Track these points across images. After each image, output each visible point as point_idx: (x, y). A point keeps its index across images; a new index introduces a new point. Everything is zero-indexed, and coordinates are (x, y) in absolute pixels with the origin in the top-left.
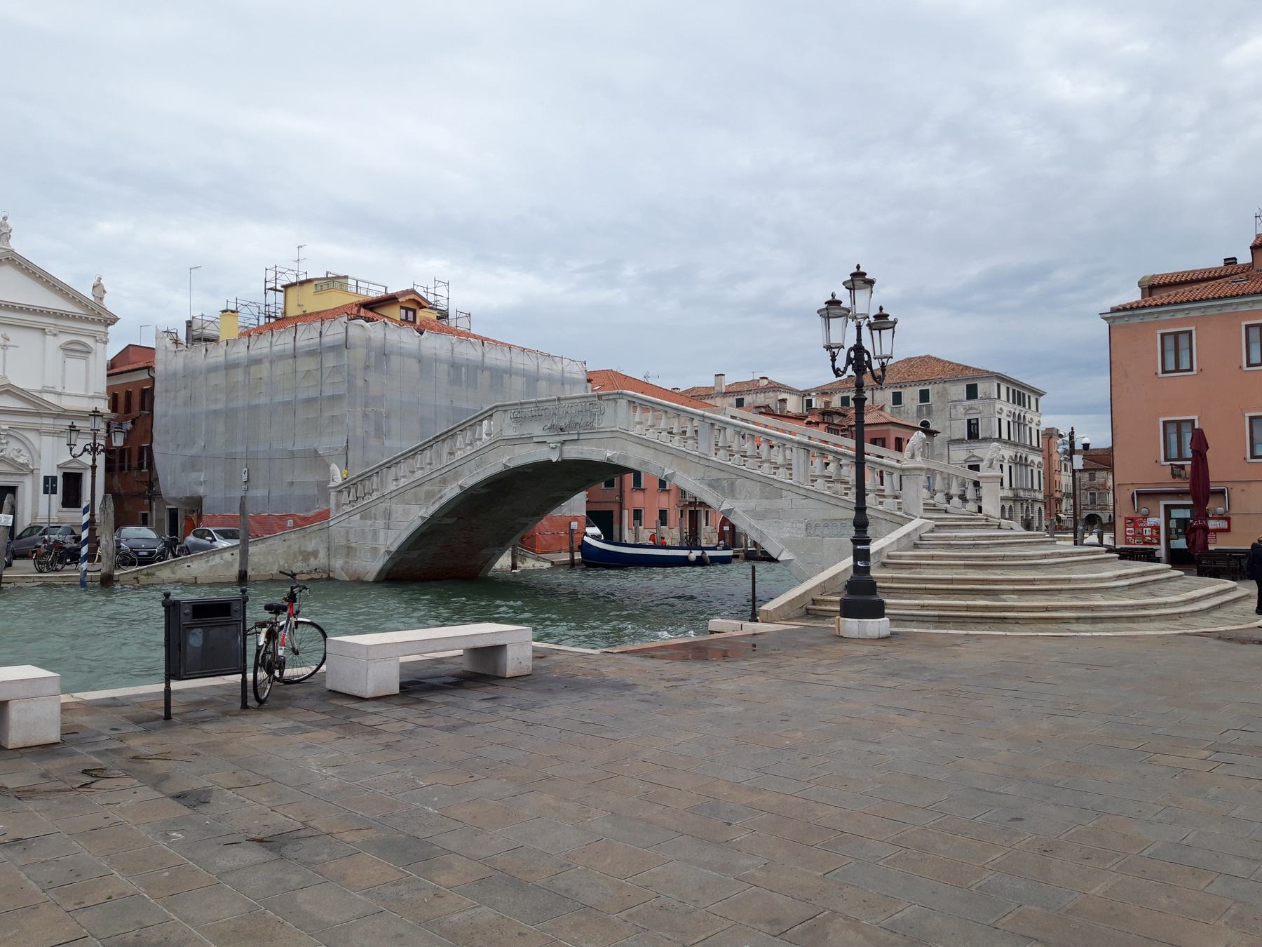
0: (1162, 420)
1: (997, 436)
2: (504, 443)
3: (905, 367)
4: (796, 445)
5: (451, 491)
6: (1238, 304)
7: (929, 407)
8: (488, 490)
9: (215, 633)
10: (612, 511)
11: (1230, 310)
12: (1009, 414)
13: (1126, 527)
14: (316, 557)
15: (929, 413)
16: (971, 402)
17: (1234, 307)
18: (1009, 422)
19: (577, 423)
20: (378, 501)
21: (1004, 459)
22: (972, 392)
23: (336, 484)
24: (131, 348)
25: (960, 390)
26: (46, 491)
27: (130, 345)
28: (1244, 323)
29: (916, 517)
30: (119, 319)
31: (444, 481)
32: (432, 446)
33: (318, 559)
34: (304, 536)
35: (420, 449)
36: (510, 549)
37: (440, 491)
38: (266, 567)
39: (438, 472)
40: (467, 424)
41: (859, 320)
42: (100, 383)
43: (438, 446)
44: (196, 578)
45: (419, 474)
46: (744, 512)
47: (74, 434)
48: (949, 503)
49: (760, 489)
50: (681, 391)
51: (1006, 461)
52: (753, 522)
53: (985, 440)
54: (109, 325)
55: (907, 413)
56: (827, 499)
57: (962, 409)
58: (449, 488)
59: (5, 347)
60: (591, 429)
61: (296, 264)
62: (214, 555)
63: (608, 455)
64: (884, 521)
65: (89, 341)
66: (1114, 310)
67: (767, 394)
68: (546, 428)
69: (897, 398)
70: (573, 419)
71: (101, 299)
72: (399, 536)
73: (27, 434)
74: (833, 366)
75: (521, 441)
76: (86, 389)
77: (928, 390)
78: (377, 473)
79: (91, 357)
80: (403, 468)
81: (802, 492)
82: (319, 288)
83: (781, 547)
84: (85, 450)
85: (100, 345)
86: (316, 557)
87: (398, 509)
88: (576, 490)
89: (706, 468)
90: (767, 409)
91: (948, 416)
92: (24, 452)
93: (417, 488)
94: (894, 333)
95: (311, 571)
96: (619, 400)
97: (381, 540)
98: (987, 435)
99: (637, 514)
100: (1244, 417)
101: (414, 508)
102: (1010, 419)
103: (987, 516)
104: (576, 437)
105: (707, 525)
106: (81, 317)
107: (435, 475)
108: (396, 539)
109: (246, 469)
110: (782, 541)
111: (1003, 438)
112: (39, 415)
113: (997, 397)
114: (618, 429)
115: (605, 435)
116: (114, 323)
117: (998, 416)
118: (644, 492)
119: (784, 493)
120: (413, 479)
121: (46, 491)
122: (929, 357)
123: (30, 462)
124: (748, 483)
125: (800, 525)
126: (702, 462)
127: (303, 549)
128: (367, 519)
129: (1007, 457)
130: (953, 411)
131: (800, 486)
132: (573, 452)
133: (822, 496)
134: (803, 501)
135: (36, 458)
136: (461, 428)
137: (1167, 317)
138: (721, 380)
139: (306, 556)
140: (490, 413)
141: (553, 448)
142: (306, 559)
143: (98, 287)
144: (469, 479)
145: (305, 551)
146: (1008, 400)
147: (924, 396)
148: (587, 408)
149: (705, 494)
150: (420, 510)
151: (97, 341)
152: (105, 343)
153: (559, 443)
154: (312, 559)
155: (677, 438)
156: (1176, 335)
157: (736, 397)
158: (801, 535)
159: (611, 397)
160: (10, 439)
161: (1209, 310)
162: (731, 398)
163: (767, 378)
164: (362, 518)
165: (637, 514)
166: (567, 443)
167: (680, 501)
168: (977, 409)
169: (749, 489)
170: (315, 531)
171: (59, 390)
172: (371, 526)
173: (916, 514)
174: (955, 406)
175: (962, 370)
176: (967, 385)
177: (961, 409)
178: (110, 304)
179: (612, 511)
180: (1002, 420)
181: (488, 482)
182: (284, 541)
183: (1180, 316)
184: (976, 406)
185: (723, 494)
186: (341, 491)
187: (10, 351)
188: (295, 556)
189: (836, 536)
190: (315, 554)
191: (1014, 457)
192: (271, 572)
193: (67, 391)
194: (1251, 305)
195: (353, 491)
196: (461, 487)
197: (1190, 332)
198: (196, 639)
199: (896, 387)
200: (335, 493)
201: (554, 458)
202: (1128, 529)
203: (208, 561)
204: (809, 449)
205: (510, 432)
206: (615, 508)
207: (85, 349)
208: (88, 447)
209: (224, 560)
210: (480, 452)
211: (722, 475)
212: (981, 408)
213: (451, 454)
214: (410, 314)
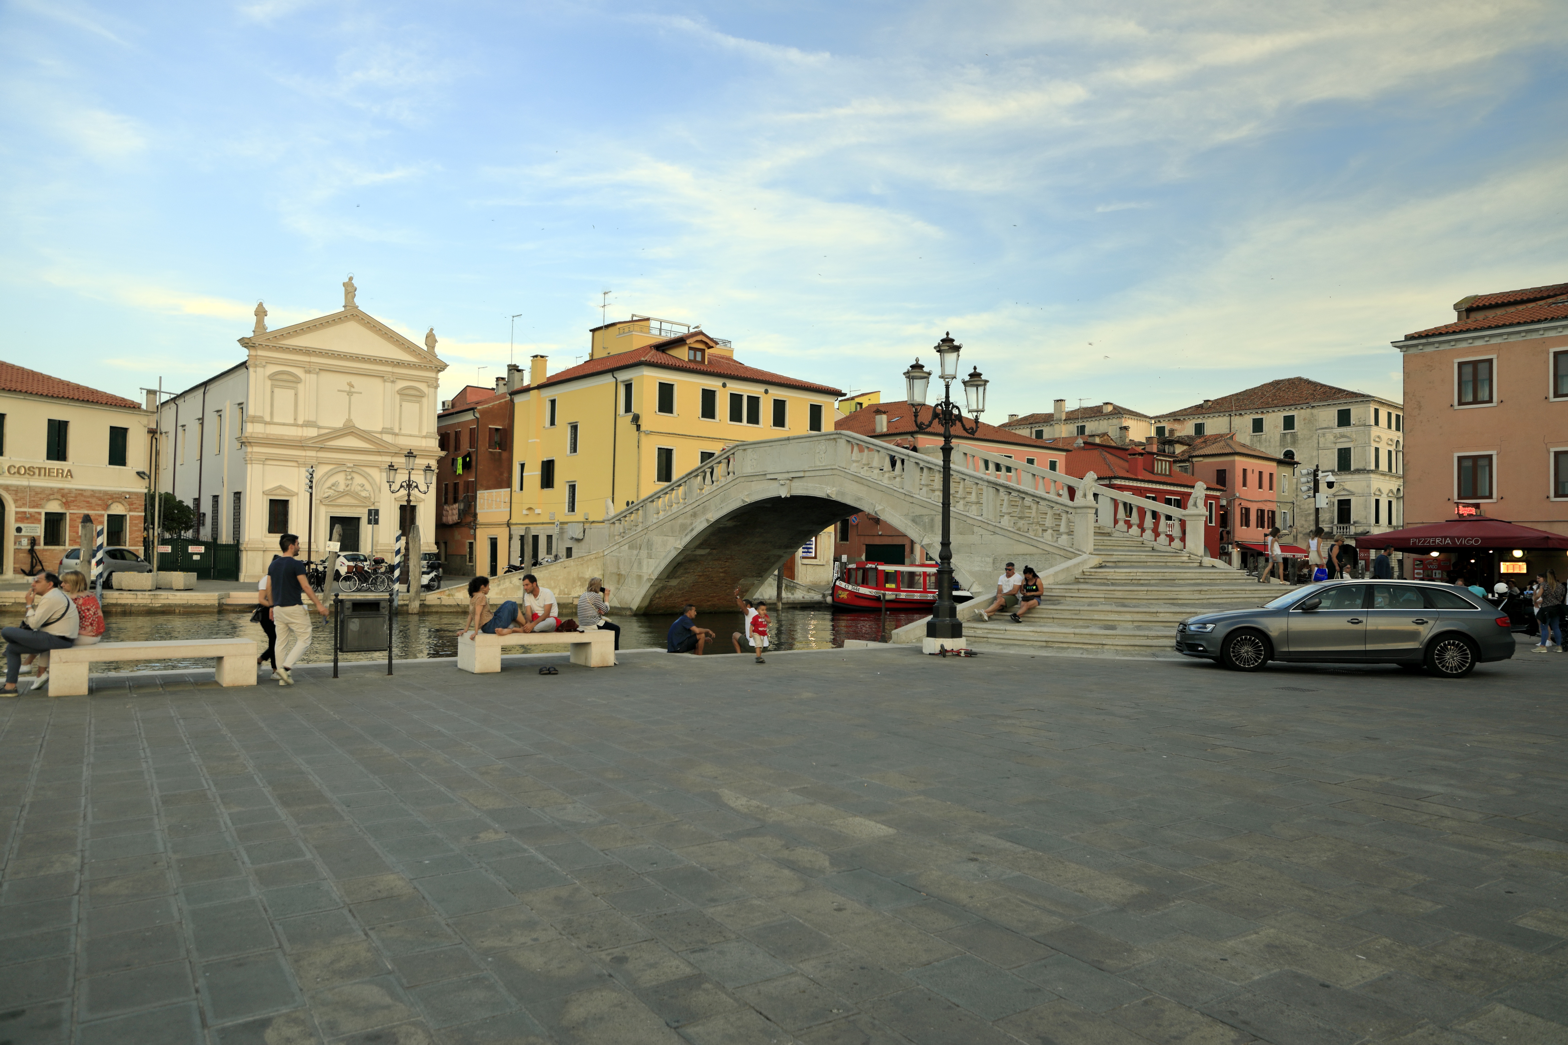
0: (1456, 455)
1: (1373, 467)
3: (1271, 391)
4: (986, 484)
5: (700, 525)
6: (1545, 329)
7: (1294, 436)
9: (368, 621)
10: (904, 545)
11: (1535, 336)
12: (1390, 443)
13: (1414, 569)
15: (1294, 441)
16: (1343, 430)
17: (1541, 332)
18: (1390, 452)
21: (1382, 493)
22: (1344, 419)
24: (468, 388)
25: (1328, 415)
26: (369, 522)
27: (467, 386)
28: (1457, 361)
29: (1085, 553)
31: (695, 515)
32: (685, 482)
34: (582, 564)
37: (692, 524)
41: (947, 380)
42: (431, 426)
47: (392, 472)
48: (1156, 540)
50: (1019, 417)
51: (1384, 495)
53: (1358, 471)
54: (439, 371)
55: (1269, 442)
56: (1011, 535)
57: (1332, 437)
58: (699, 521)
59: (350, 394)
61: (603, 309)
64: (1058, 556)
66: (1409, 338)
67: (1110, 421)
69: (1258, 426)
71: (433, 347)
73: (368, 470)
74: (916, 421)
75: (757, 478)
76: (420, 430)
77: (1293, 416)
79: (425, 400)
81: (990, 528)
82: (621, 331)
83: (972, 579)
84: (402, 486)
87: (657, 540)
89: (911, 505)
90: (1106, 437)
91: (1316, 445)
92: (368, 486)
94: (984, 390)
97: (645, 569)
98: (1360, 466)
100: (1549, 452)
101: (671, 540)
102: (1393, 448)
103: (1190, 553)
107: (687, 509)
108: (656, 568)
112: (379, 453)
113: (1372, 422)
115: (826, 473)
117: (1375, 445)
119: (976, 529)
120: (670, 513)
121: (369, 522)
122: (1300, 379)
123: (372, 495)
125: (988, 559)
126: (907, 498)
127: (581, 575)
129: (1385, 491)
130: (1322, 440)
131: (989, 522)
133: (1006, 532)
134: (991, 537)
135: (377, 491)
137: (1464, 345)
138: (1061, 406)
140: (732, 452)
143: (431, 339)
144: (714, 515)
145: (583, 578)
146: (1390, 427)
147: (1289, 423)
153: (788, 479)
156: (1475, 363)
157: (1076, 425)
159: (832, 437)
160: (354, 475)
161: (1513, 336)
162: (1072, 425)
163: (1111, 404)
164: (630, 548)
166: (795, 480)
168: (1348, 437)
171: (397, 431)
173: (1085, 550)
174: (1324, 434)
175: (1334, 393)
176: (1339, 411)
177: (1330, 437)
178: (441, 351)
179: (904, 545)
180: (1387, 427)
183: (1479, 343)
184: (1348, 435)
186: (614, 523)
187: (355, 397)
191: (1395, 491)
193: (403, 432)
194: (1560, 330)
196: (707, 520)
197: (1490, 361)
198: (354, 625)
199: (1257, 413)
202: (1416, 571)
203: (499, 585)
204: (997, 487)
207: (418, 393)
208: (404, 484)
210: (724, 488)
211: (924, 511)
212: (1354, 436)
214: (699, 355)
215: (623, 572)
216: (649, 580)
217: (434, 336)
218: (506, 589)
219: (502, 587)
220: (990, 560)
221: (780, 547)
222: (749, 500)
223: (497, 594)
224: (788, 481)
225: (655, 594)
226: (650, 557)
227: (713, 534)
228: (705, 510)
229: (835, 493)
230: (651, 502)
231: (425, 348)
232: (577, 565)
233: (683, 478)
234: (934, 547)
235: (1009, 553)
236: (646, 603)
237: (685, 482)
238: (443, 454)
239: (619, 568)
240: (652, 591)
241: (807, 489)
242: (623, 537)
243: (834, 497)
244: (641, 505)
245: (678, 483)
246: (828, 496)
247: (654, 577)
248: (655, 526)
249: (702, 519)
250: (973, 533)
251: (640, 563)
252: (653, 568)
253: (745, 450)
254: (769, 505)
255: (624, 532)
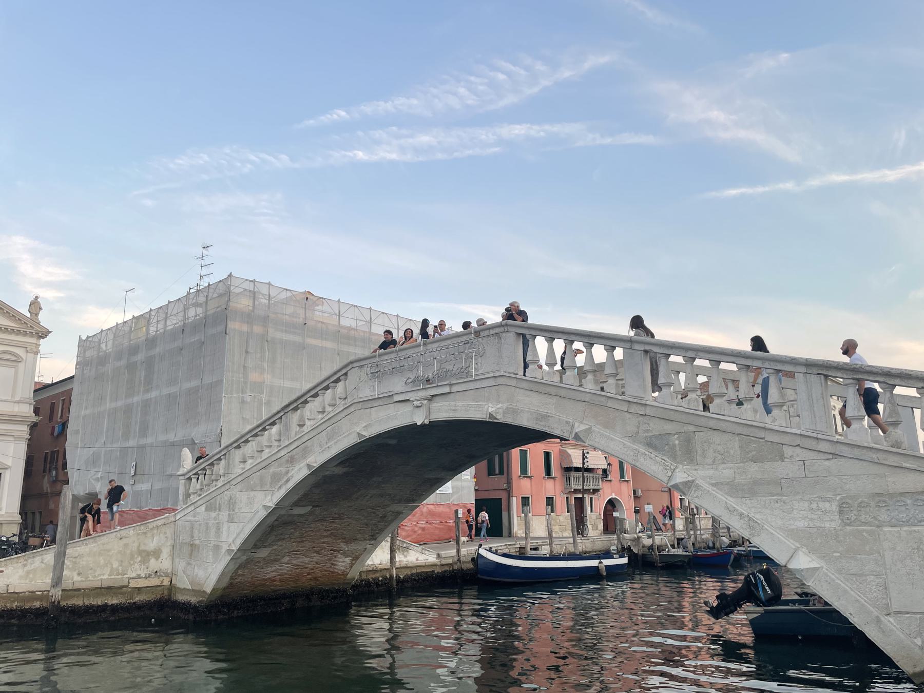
2: (360, 406)
4: (803, 369)
5: (299, 473)
8: (345, 470)
14: (157, 558)
19: (447, 372)
20: (223, 489)
23: (186, 470)
30: (51, 332)
31: (292, 460)
32: (281, 418)
33: (160, 560)
35: (269, 423)
36: (389, 539)
37: (287, 472)
38: (95, 571)
39: (285, 449)
40: (319, 388)
43: (287, 417)
44: (8, 586)
45: (266, 453)
46: (713, 485)
49: (741, 447)
52: (732, 502)
60: (467, 377)
62: (33, 557)
63: (490, 410)
65: (20, 352)
68: (409, 381)
70: (443, 366)
71: (37, 315)
72: (242, 530)
75: (380, 402)
76: (13, 396)
78: (225, 454)
79: (21, 366)
80: (250, 448)
81: (823, 446)
83: (792, 544)
85: (31, 356)
86: (157, 558)
88: (455, 469)
89: (641, 419)
93: (263, 471)
95: (150, 575)
96: (504, 334)
97: (224, 537)
99: (525, 501)
101: (259, 495)
104: (447, 390)
105: (592, 511)
106: (7, 329)
107: (282, 453)
108: (238, 535)
109: (134, 463)
110: (793, 534)
111: (838, 431)
114: (502, 373)
116: (47, 336)
118: (531, 479)
119: (788, 451)
120: (259, 460)
124: (716, 438)
127: (142, 548)
128: (212, 511)
131: (820, 436)
132: (444, 411)
134: (827, 463)
136: (313, 393)
139: (146, 555)
140: (344, 371)
141: (418, 407)
142: (144, 561)
144: (318, 458)
145: (144, 551)
148: (461, 349)
149: (642, 460)
150: (266, 497)
151: (27, 351)
152: (36, 353)
154: (153, 561)
155: (590, 377)
158: (832, 523)
159: (492, 332)
164: (206, 510)
165: (525, 501)
167: (565, 489)
169: (720, 448)
170: (158, 527)
172: (215, 519)
178: (44, 319)
181: (343, 459)
182: (121, 539)
185: (674, 457)
188: (132, 557)
189: (908, 523)
190: (157, 553)
192: (102, 577)
195: (201, 477)
196: (309, 466)
200: (183, 481)
201: (420, 419)
203: (25, 565)
205: (366, 392)
206: (503, 495)
209: (46, 564)
210: (332, 421)
211: (668, 427)
213: (301, 426)
215: (197, 542)
216: (229, 551)
217: (39, 304)
218: (34, 571)
219: (28, 568)
220: (834, 507)
221: (400, 502)
222: (368, 434)
223: (21, 577)
224: (426, 402)
225: (238, 569)
226: (231, 520)
227: (316, 485)
228: (306, 452)
229: (501, 411)
230: (235, 448)
231: (28, 315)
232: (138, 535)
233: (278, 412)
234: (698, 486)
235: (877, 491)
236: (225, 582)
237: (281, 418)
238: (35, 419)
239: (192, 537)
240: (232, 568)
241: (455, 410)
242: (200, 495)
243: (501, 418)
244: (223, 453)
245: (271, 421)
246: (491, 415)
247: (235, 547)
248: (240, 479)
249: (302, 465)
250: (782, 458)
251: (218, 529)
252: (235, 535)
253: (362, 366)
254: (393, 442)
255: (201, 490)
